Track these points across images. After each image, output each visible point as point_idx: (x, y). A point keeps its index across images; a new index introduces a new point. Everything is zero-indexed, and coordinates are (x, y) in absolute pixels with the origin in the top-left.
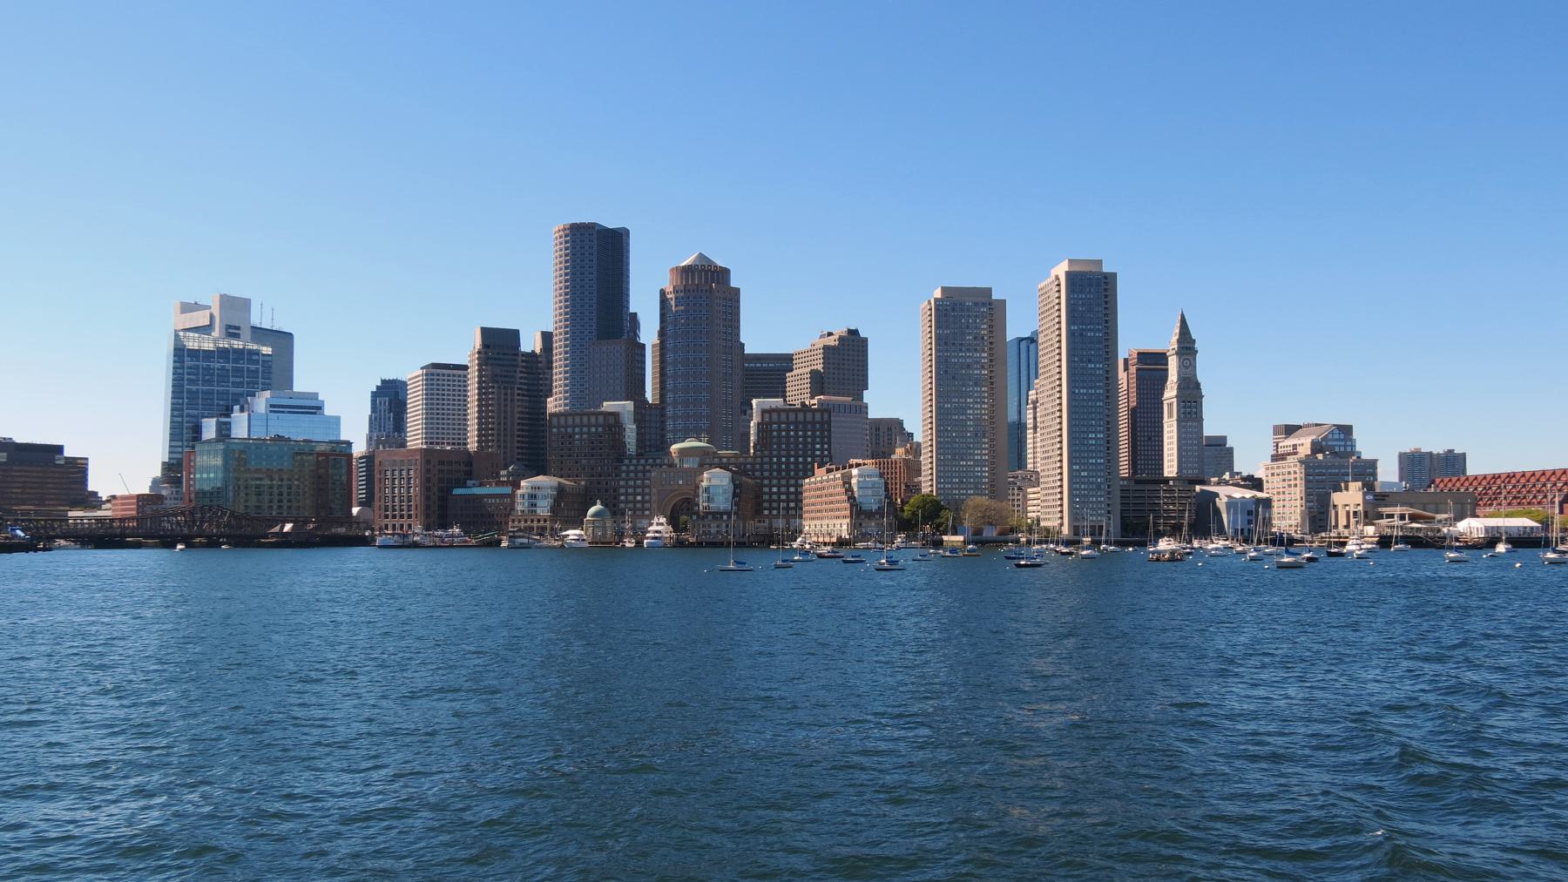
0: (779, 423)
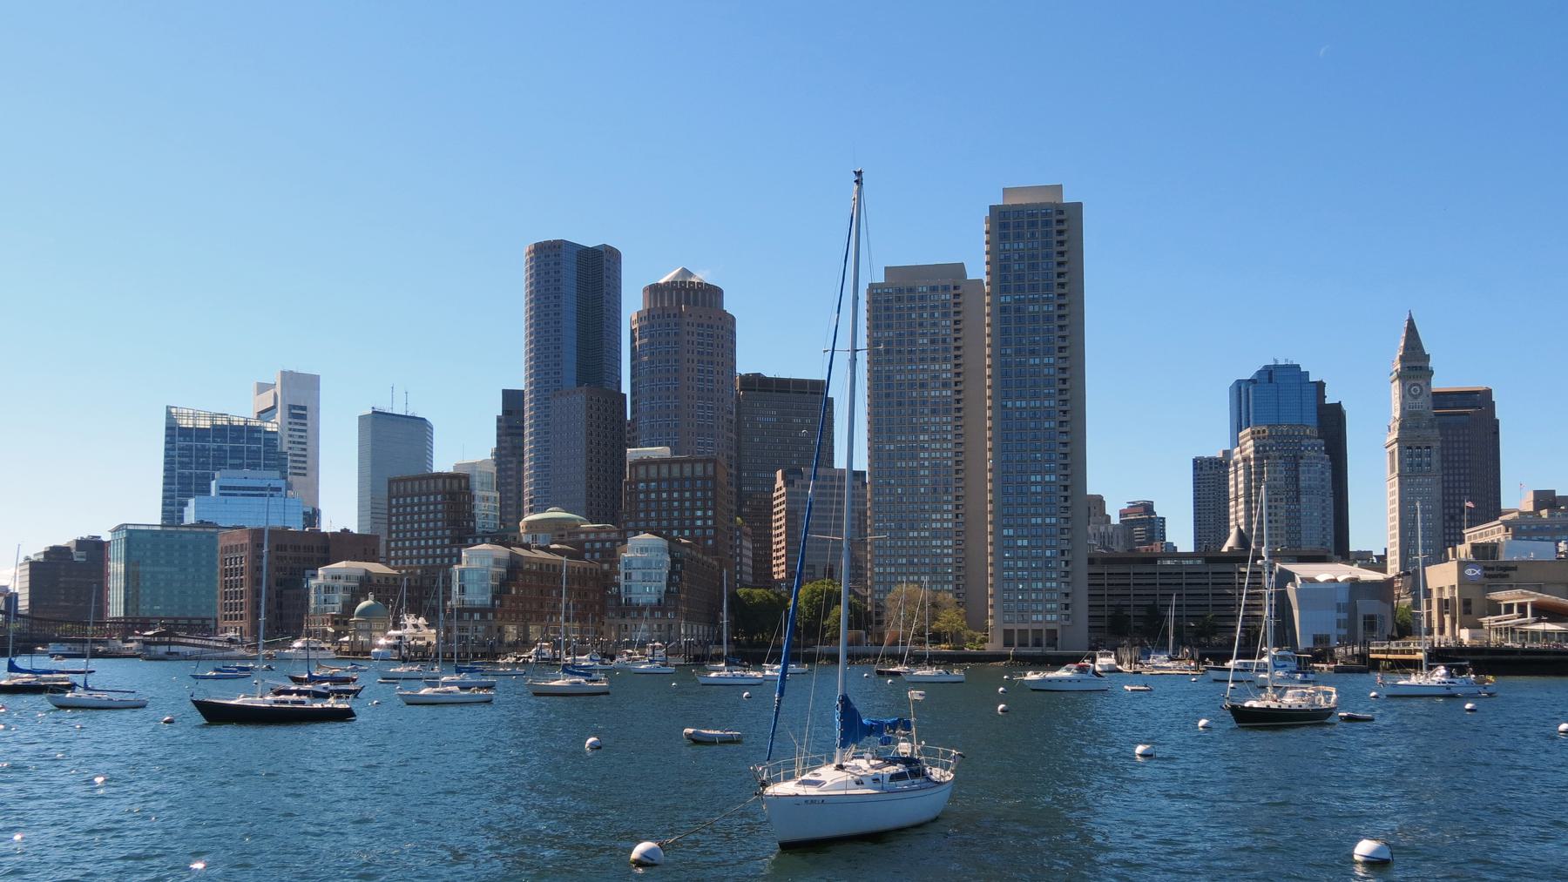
0: (648, 481)
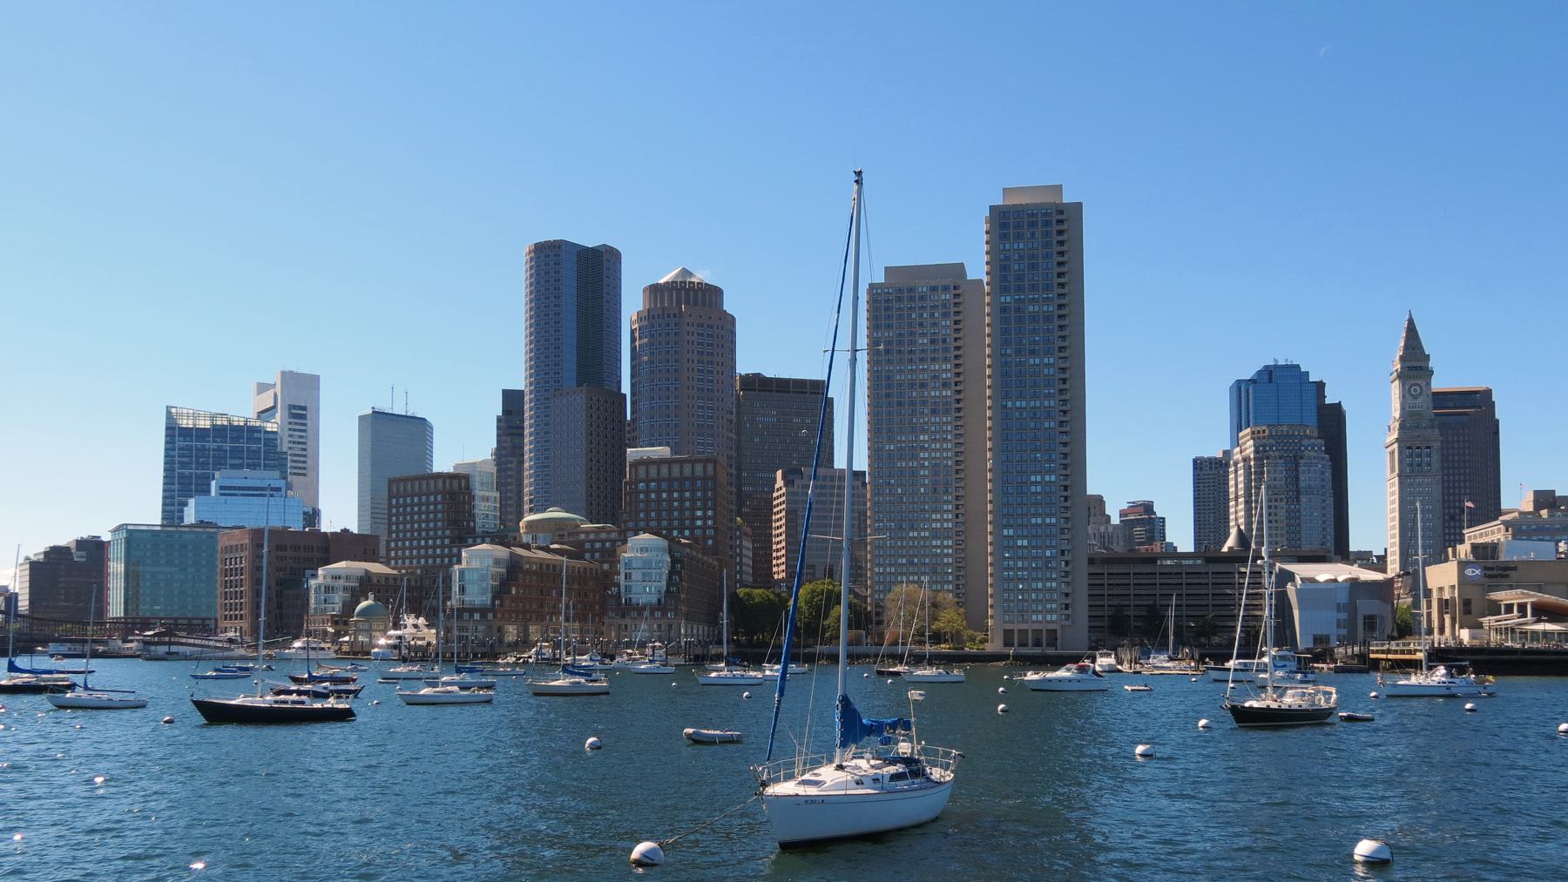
0: (648, 481)
